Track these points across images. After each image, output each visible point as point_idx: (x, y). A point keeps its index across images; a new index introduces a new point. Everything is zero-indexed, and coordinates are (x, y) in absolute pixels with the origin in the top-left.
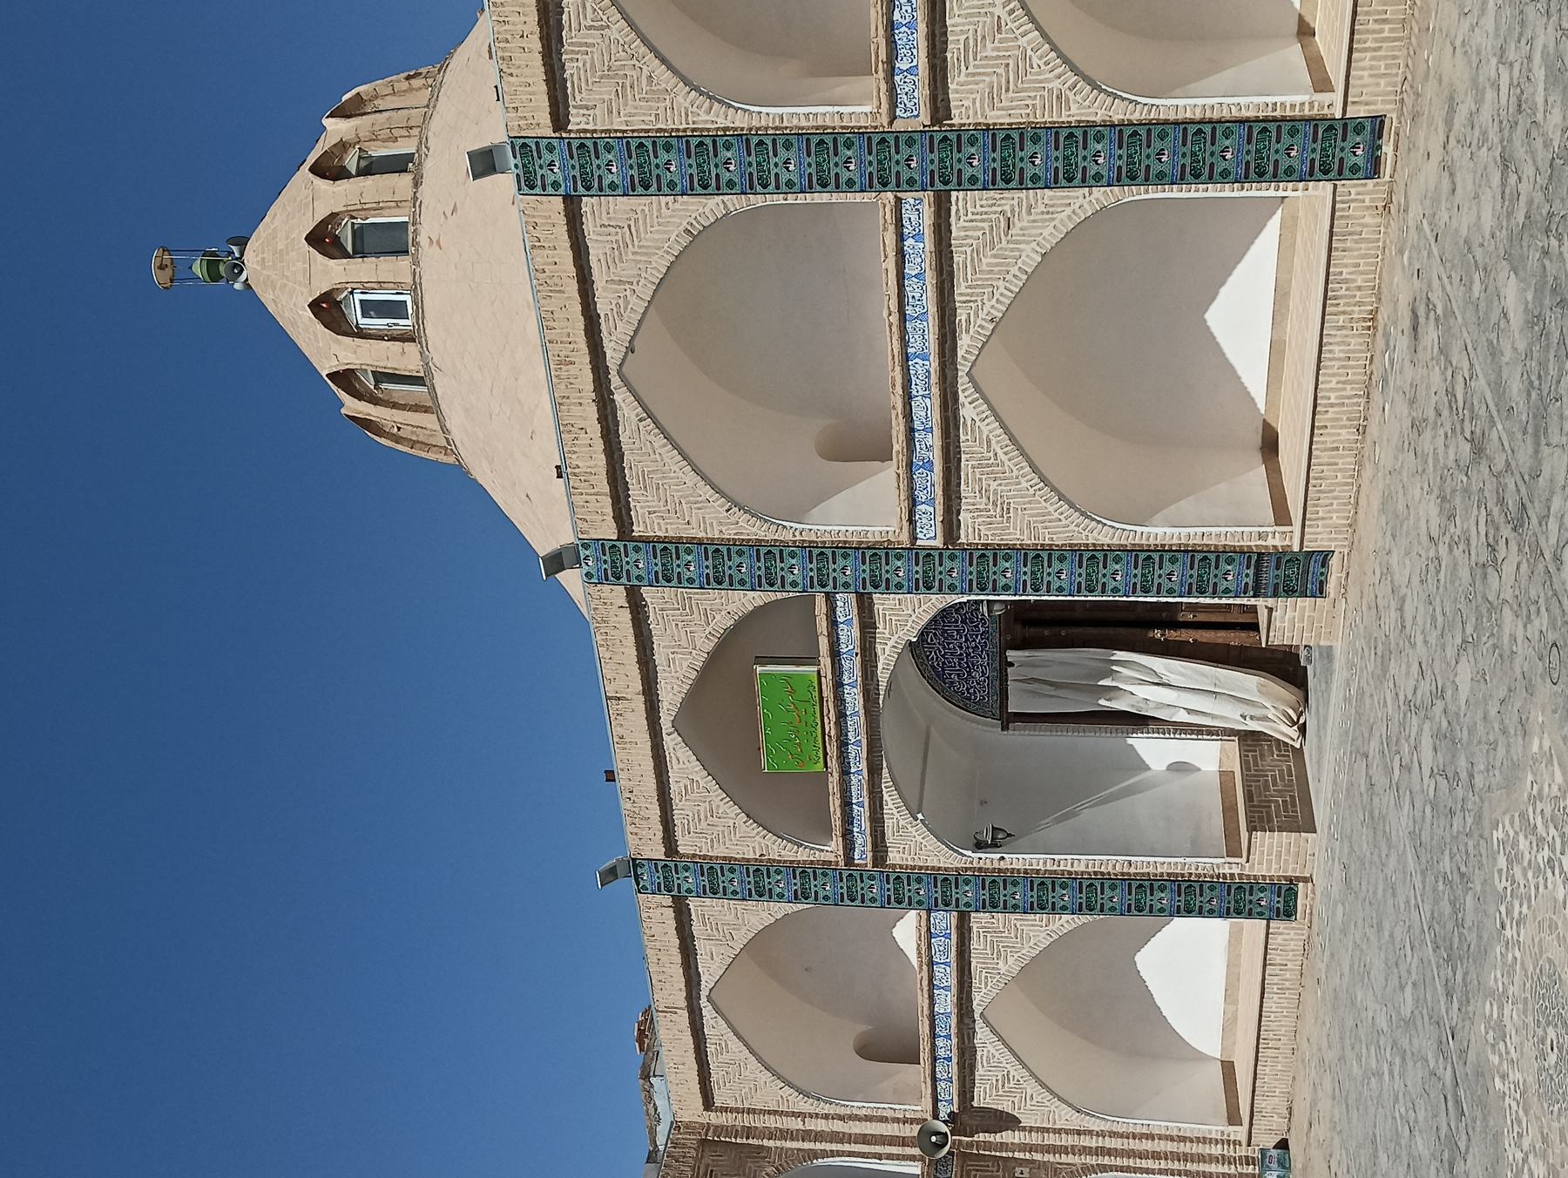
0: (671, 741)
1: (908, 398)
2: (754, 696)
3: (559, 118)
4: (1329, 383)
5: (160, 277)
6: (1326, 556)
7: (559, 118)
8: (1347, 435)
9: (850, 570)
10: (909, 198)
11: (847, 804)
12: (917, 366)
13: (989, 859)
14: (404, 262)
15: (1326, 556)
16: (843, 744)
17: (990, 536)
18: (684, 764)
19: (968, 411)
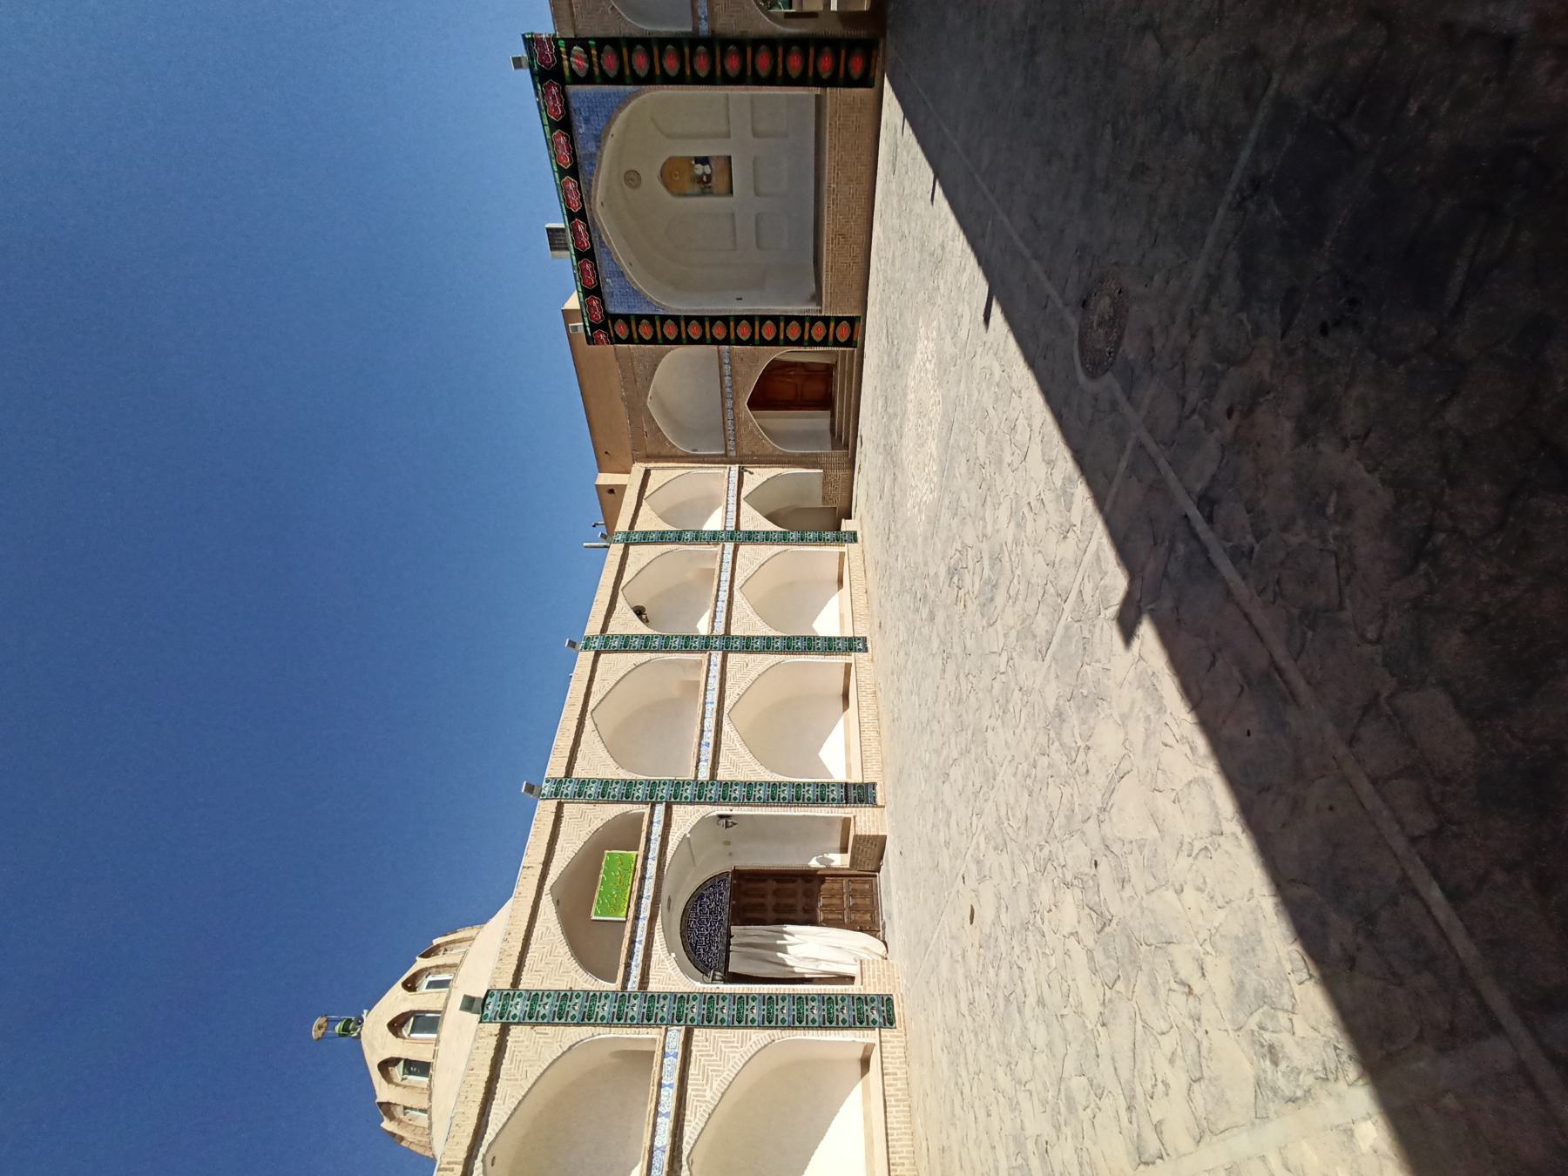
0: (547, 902)
1: (703, 718)
2: (600, 867)
3: (560, 806)
4: (863, 715)
5: (316, 1033)
6: (874, 785)
7: (560, 806)
8: (873, 734)
9: (664, 792)
10: (714, 653)
11: (648, 840)
12: (709, 707)
13: (725, 810)
14: (426, 1080)
15: (874, 785)
16: (640, 897)
17: (728, 778)
18: (547, 902)
19: (726, 727)
